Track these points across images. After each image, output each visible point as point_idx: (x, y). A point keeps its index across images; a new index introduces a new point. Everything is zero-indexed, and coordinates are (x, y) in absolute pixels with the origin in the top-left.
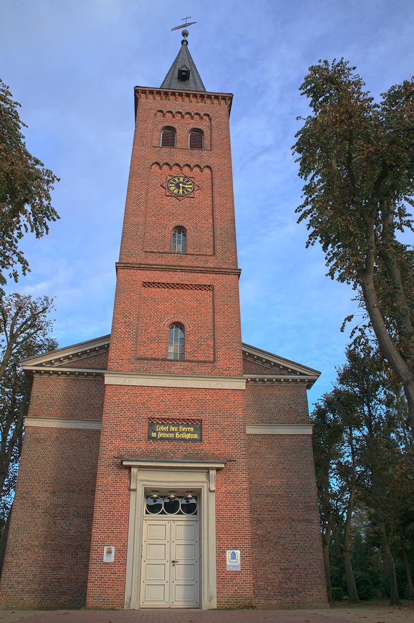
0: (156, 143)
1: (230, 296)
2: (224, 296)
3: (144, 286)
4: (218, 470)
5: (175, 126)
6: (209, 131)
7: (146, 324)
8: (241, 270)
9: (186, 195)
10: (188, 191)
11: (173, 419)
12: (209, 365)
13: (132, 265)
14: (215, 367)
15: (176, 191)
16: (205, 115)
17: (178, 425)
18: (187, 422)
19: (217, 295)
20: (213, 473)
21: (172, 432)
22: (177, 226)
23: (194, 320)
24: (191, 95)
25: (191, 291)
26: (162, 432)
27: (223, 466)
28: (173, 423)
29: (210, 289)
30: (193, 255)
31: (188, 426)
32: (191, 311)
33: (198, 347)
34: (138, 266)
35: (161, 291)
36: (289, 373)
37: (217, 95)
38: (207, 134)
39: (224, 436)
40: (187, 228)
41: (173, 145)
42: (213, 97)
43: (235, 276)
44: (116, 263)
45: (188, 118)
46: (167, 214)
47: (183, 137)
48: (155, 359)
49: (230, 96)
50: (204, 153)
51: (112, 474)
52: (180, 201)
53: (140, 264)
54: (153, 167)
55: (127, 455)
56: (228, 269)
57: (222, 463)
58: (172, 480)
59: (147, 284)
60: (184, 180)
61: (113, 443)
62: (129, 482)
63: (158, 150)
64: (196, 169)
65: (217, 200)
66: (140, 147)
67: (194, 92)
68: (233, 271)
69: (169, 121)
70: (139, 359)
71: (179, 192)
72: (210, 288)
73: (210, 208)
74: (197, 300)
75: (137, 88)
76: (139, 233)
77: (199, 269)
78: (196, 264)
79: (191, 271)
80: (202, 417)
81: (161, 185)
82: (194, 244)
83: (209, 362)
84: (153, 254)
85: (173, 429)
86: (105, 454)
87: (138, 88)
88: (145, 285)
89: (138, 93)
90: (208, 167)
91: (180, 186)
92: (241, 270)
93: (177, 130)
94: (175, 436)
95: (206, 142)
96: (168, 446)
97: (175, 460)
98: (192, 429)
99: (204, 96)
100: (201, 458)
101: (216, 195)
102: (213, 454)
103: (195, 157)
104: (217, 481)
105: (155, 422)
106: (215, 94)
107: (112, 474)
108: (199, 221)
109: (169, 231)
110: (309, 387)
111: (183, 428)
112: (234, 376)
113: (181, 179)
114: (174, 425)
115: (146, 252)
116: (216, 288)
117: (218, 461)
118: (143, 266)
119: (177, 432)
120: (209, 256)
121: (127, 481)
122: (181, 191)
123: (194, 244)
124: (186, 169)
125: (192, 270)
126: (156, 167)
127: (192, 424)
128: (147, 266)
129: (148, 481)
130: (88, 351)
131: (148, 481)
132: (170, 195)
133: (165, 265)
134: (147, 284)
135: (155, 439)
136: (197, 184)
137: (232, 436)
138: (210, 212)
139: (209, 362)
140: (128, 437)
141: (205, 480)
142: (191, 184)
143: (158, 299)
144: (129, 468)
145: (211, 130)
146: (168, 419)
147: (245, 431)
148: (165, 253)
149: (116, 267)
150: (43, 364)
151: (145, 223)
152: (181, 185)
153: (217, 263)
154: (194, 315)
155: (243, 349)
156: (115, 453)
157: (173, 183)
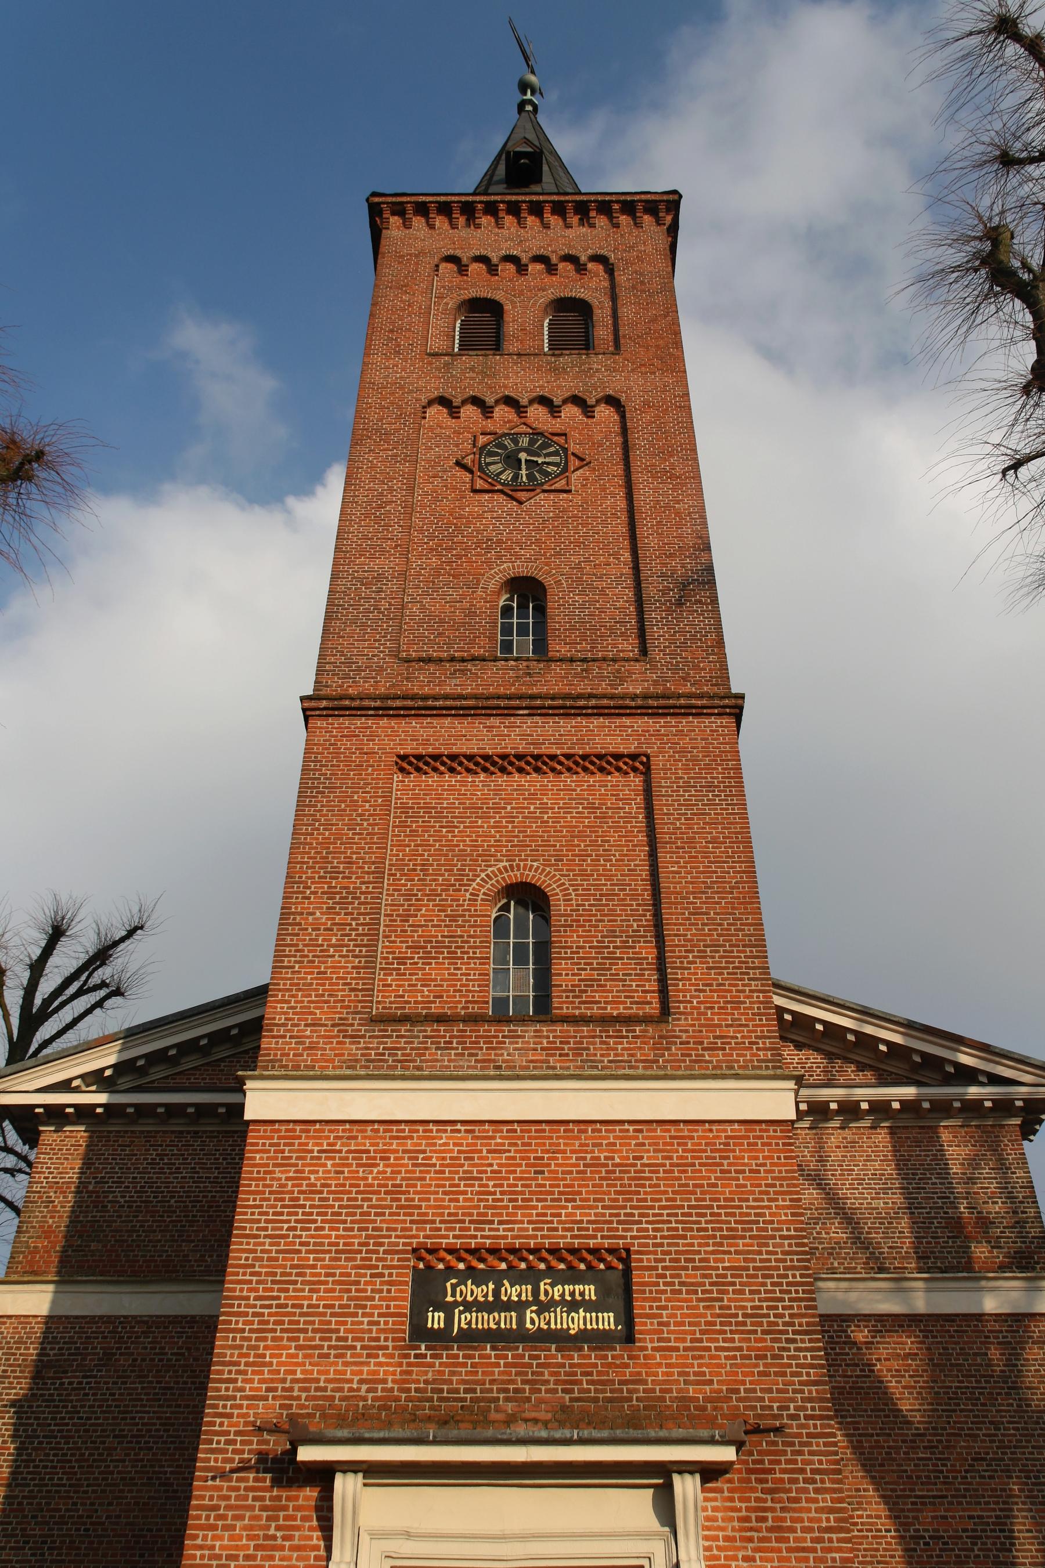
0: (436, 344)
1: (710, 787)
2: (687, 786)
3: (402, 770)
4: (709, 1472)
5: (499, 296)
6: (608, 304)
7: (409, 895)
8: (742, 697)
9: (542, 484)
10: (547, 474)
11: (512, 1251)
12: (653, 1032)
13: (357, 703)
14: (669, 1038)
15: (507, 476)
16: (597, 258)
17: (531, 1276)
18: (571, 1261)
19: (663, 784)
20: (686, 1488)
21: (508, 1306)
22: (513, 579)
23: (584, 874)
24: (547, 208)
25: (568, 779)
26: (468, 1307)
27: (727, 1454)
28: (511, 1267)
29: (635, 769)
30: (572, 660)
31: (573, 1276)
32: (570, 846)
33: (601, 968)
34: (378, 703)
35: (463, 783)
36: (948, 1080)
37: (629, 198)
38: (602, 314)
39: (726, 1316)
40: (548, 581)
41: (497, 345)
42: (616, 206)
43: (725, 720)
44: (303, 699)
45: (540, 273)
46: (478, 544)
47: (527, 314)
48: (441, 1019)
49: (671, 197)
50: (597, 362)
51: (252, 1508)
52: (521, 503)
53: (387, 698)
54: (432, 411)
55: (324, 1416)
56: (701, 696)
57: (725, 1442)
58: (515, 1526)
59: (411, 763)
60: (532, 442)
61: (264, 1364)
62: (322, 1543)
63: (446, 364)
64: (571, 411)
65: (644, 495)
66: (388, 359)
67: (556, 198)
68: (717, 702)
69: (478, 284)
70: (375, 1020)
71: (516, 477)
72: (638, 763)
73: (624, 517)
74: (592, 807)
75: (376, 200)
76: (384, 605)
77: (593, 702)
78: (582, 687)
79: (567, 712)
80: (628, 1237)
81: (458, 463)
82: (573, 628)
83: (647, 1020)
84: (432, 667)
85: (512, 1292)
86: (230, 1416)
87: (381, 200)
88: (405, 765)
89: (380, 213)
90: (612, 401)
91: (520, 461)
92: (742, 697)
93: (508, 307)
94: (521, 1321)
95: (602, 332)
96: (494, 1365)
97: (521, 1430)
98: (590, 1291)
99: (587, 208)
100: (633, 1421)
101: (640, 478)
102: (684, 1401)
103: (567, 377)
104: (708, 1524)
105: (441, 1266)
106: (623, 198)
107: (252, 1508)
108: (587, 561)
109: (489, 594)
110: (1028, 1131)
111: (553, 1285)
112: (745, 1067)
113: (524, 442)
114: (519, 1278)
115: (407, 661)
116: (658, 762)
117: (704, 1433)
118: (398, 703)
119: (527, 1304)
120: (628, 660)
121: (316, 1538)
122: (524, 472)
123: (573, 628)
124: (537, 414)
125: (568, 707)
126: (436, 412)
127: (590, 1267)
128: (409, 703)
129: (408, 1535)
130: (234, 1032)
131: (408, 1535)
132: (486, 486)
133: (476, 697)
134: (411, 763)
135: (440, 1338)
136: (576, 452)
137: (755, 1315)
138: (623, 529)
139: (647, 1020)
140: (326, 1332)
141: (649, 1520)
142: (556, 454)
143: (451, 807)
144: (323, 1476)
145: (614, 298)
146: (494, 1251)
147: (811, 1299)
148: (474, 659)
149: (304, 710)
150: (75, 1083)
151: (404, 575)
152: (523, 456)
153: (656, 683)
154: (583, 856)
155: (779, 1001)
156: (269, 1410)
157: (496, 454)
